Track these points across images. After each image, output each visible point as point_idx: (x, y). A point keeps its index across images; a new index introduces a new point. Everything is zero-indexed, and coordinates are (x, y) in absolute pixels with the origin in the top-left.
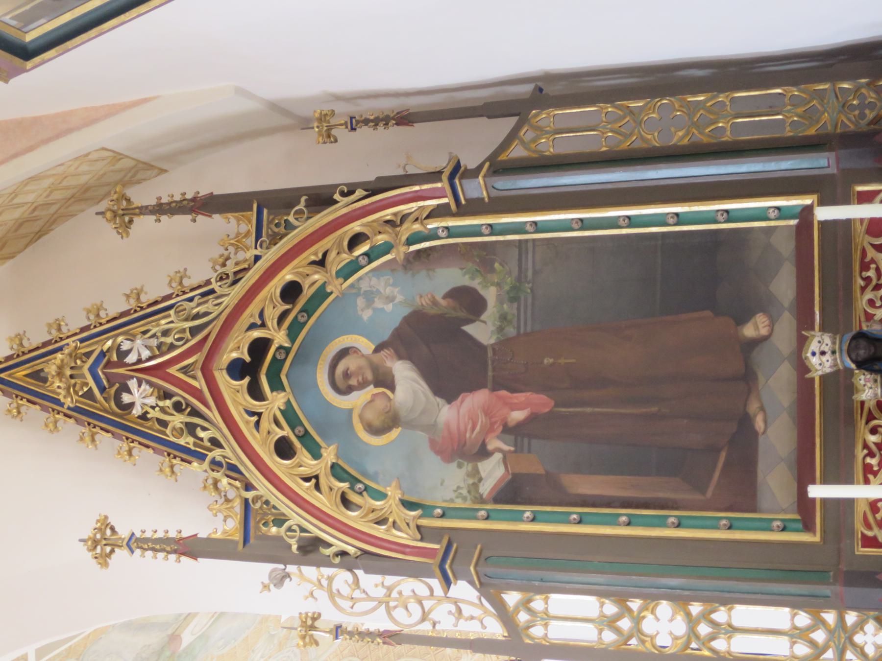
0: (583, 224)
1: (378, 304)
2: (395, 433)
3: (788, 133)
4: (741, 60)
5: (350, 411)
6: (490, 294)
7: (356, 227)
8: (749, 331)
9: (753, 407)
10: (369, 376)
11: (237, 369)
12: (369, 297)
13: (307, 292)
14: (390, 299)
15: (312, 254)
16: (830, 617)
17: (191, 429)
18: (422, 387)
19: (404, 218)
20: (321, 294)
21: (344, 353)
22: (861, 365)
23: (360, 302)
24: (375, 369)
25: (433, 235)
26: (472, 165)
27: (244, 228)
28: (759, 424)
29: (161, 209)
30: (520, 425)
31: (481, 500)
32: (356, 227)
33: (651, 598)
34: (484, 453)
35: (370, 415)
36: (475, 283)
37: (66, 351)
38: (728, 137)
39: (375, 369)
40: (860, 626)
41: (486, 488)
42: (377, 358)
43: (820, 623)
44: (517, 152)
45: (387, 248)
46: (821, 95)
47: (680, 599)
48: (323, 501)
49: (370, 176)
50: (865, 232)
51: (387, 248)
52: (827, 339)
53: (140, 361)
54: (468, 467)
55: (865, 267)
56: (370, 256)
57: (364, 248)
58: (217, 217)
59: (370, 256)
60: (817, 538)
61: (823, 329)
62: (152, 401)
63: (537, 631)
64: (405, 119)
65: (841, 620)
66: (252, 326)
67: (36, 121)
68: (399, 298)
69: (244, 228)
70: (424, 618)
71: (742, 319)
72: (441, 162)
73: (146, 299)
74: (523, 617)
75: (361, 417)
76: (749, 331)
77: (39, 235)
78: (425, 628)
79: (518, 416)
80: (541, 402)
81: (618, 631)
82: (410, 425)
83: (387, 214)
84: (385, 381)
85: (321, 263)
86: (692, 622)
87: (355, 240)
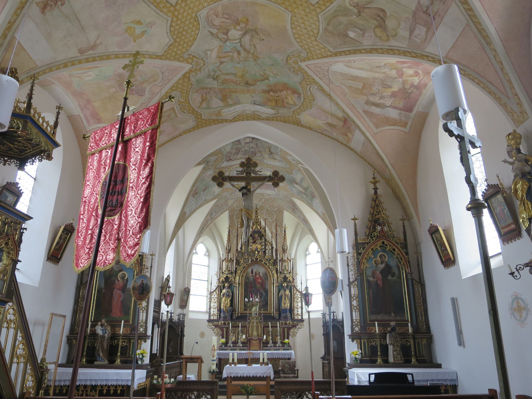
0: (405, 292)
1: (392, 262)
2: (375, 265)
3: (418, 319)
5: (377, 258)
6: (394, 278)
7: (403, 259)
8: (392, 314)
9: (383, 314)
10: (382, 260)
12: (393, 260)
14: (393, 263)
15: (399, 252)
16: (359, 324)
18: (381, 269)
19: (405, 266)
20: (394, 254)
21: (385, 257)
23: (392, 259)
24: (383, 261)
25: (402, 270)
26: (412, 276)
27: (402, 240)
28: (381, 315)
29: (404, 226)
30: (378, 283)
31: (367, 278)
32: (403, 259)
33: (358, 301)
34: (373, 278)
35: (377, 261)
36: (396, 276)
37: (384, 216)
39: (383, 261)
40: (358, 328)
41: (369, 278)
42: (385, 262)
44: (414, 282)
45: (400, 264)
46: (423, 324)
47: (359, 305)
48: (366, 256)
49: (410, 260)
50: (46, 258)
51: (400, 264)
52: (394, 324)
53: (384, 228)
54: (371, 275)
55: (402, 328)
56: (399, 261)
57: (400, 260)
58: (403, 236)
59: (399, 261)
60: (368, 322)
61: (396, 324)
62: (378, 230)
63: (352, 286)
64: (418, 265)
65: (355, 325)
66: (389, 245)
67: (417, 207)
68: (393, 265)
69: (402, 240)
70: (351, 270)
71: (394, 313)
72: (413, 271)
73: (391, 225)
74: (353, 284)
75: (376, 260)
76: (392, 314)
77: (397, 198)
78: (350, 270)
79: (379, 282)
80: (381, 286)
81: (354, 297)
82: (376, 267)
84: (382, 263)
87: (401, 259)
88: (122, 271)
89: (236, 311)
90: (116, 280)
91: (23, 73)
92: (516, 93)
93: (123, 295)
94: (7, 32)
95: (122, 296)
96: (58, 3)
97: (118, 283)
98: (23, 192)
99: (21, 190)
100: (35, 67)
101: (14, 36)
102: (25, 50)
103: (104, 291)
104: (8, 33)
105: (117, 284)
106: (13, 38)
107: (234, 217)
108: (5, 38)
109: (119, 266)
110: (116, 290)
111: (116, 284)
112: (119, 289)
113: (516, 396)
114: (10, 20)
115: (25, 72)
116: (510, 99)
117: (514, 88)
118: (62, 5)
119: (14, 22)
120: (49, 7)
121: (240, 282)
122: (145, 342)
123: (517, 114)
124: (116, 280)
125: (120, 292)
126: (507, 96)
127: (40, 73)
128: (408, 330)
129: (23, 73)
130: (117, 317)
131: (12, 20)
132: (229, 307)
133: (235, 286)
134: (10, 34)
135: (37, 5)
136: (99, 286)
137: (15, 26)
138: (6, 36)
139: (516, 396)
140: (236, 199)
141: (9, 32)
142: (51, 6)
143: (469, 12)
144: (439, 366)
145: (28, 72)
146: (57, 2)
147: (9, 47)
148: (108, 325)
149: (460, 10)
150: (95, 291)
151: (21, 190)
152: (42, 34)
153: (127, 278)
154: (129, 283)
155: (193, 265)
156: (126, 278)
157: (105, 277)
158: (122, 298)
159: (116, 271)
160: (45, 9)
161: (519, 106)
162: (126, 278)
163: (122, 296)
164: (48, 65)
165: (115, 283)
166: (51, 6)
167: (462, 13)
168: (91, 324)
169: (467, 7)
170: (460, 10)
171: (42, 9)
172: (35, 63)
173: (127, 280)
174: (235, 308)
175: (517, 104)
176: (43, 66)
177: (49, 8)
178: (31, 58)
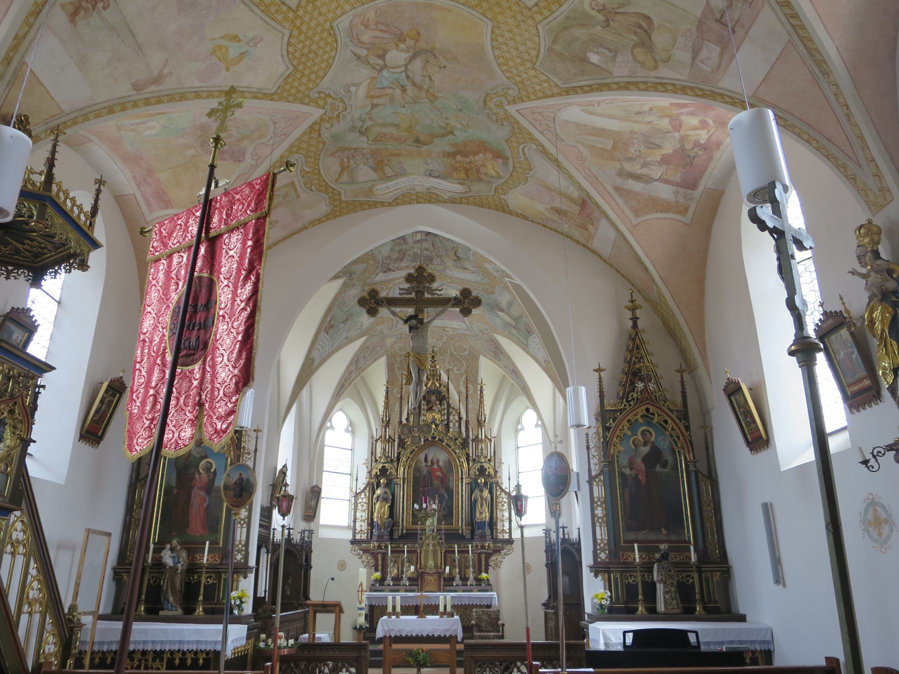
0: (684, 492)
1: (663, 442)
2: (633, 447)
4: (837, 575)
5: (637, 435)
6: (667, 470)
7: (681, 438)
8: (663, 530)
9: (647, 530)
10: (646, 440)
11: (647, 410)
12: (664, 440)
13: (666, 426)
14: (664, 445)
15: (675, 426)
16: (607, 547)
17: (633, 399)
18: (644, 454)
20: (665, 428)
21: (651, 433)
22: (662, 555)
23: (663, 437)
24: (648, 441)
25: (680, 456)
26: (697, 466)
27: (679, 406)
28: (643, 532)
29: (682, 382)
30: (638, 478)
31: (621, 469)
32: (681, 438)
33: (606, 509)
34: (631, 469)
35: (637, 441)
36: (669, 466)
38: (705, 525)
39: (648, 441)
40: (605, 553)
41: (623, 470)
42: (650, 442)
43: (243, 547)
44: (700, 476)
45: (677, 445)
47: (606, 515)
48: (618, 432)
49: (693, 440)
51: (677, 445)
52: (666, 548)
53: (649, 386)
54: (628, 465)
56: (674, 440)
57: (677, 440)
58: (681, 398)
59: (674, 440)
60: (622, 544)
61: (669, 547)
62: (639, 389)
63: (595, 483)
64: (707, 448)
65: (599, 550)
66: (657, 413)
67: (705, 350)
68: (664, 447)
69: (679, 406)
71: (665, 528)
72: (697, 458)
73: (660, 380)
74: (597, 480)
75: (636, 438)
76: (663, 530)
78: (591, 456)
79: (640, 477)
80: (644, 483)
81: (598, 501)
82: (635, 450)
83: (685, 445)
84: (645, 444)
85: (673, 429)
86: (601, 518)
87: (678, 437)
88: (205, 457)
89: (399, 526)
90: (196, 473)
91: (40, 123)
92: (872, 157)
93: (207, 498)
94: (11, 54)
95: (205, 500)
96: (98, 5)
97: (199, 478)
98: (38, 325)
99: (36, 321)
100: (60, 114)
101: (24, 62)
102: (42, 84)
103: (175, 491)
104: (14, 57)
105: (198, 479)
106: (22, 64)
107: (396, 366)
108: (9, 64)
109: (201, 449)
110: (197, 490)
111: (196, 480)
112: (200, 489)
113: (872, 669)
114: (17, 34)
115: (42, 122)
116: (861, 168)
117: (868, 148)
118: (104, 8)
119: (24, 37)
120: (83, 12)
121: (406, 476)
122: (245, 578)
123: (874, 193)
124: (196, 473)
125: (203, 493)
126: (856, 161)
127: (67, 123)
128: (690, 558)
129: (40, 123)
130: (198, 535)
131: (21, 34)
132: (387, 519)
133: (397, 484)
134: (17, 57)
135: (63, 9)
136: (167, 482)
137: (26, 43)
138: (11, 61)
139: (872, 669)
140: (399, 336)
141: (15, 54)
142: (86, 10)
143: (792, 20)
144: (742, 618)
145: (48, 121)
146: (96, 4)
147: (16, 79)
148: (183, 549)
149: (778, 17)
150: (160, 491)
151: (36, 321)
152: (72, 58)
153: (215, 470)
154: (217, 478)
155: (325, 447)
156: (212, 470)
157: (177, 468)
158: (206, 503)
159: (195, 457)
160: (76, 15)
161: (877, 178)
162: (212, 470)
163: (205, 500)
164: (81, 110)
165: (194, 478)
166: (86, 10)
167: (781, 22)
168: (154, 548)
169: (789, 11)
170: (778, 17)
171: (71, 14)
172: (59, 106)
173: (215, 473)
174: (398, 520)
175: (874, 176)
176: (73, 112)
177: (82, 13)
178: (52, 97)
